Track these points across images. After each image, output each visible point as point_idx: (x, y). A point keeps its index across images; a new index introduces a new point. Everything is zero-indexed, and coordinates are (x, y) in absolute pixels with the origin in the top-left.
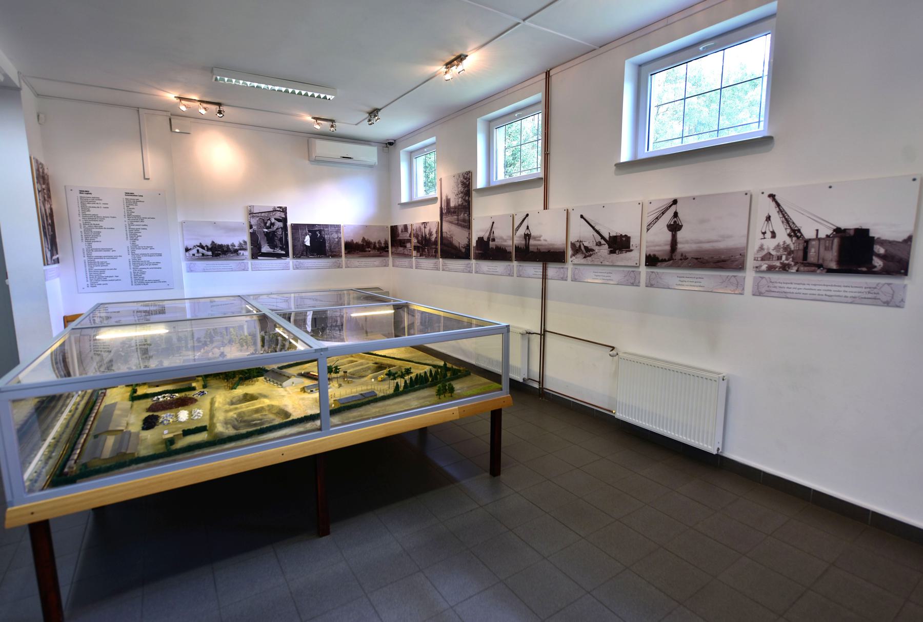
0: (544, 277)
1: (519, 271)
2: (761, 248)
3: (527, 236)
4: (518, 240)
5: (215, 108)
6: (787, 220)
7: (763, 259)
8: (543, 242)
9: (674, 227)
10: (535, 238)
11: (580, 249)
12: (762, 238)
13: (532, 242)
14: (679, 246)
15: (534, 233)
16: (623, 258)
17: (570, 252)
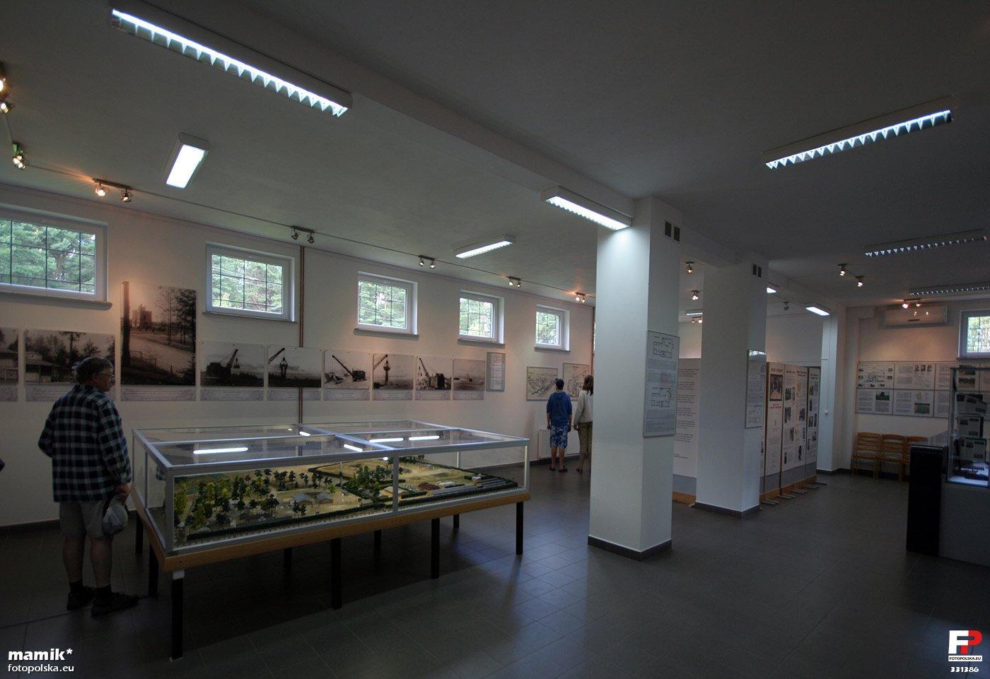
0: (301, 399)
1: (454, 396)
2: (418, 380)
3: (284, 367)
4: (273, 367)
5: (516, 281)
6: (425, 370)
7: (419, 384)
8: (301, 372)
9: (387, 369)
10: (292, 368)
11: (330, 378)
12: (417, 377)
13: (288, 371)
14: (389, 378)
15: (290, 363)
16: (361, 384)
17: (323, 380)
